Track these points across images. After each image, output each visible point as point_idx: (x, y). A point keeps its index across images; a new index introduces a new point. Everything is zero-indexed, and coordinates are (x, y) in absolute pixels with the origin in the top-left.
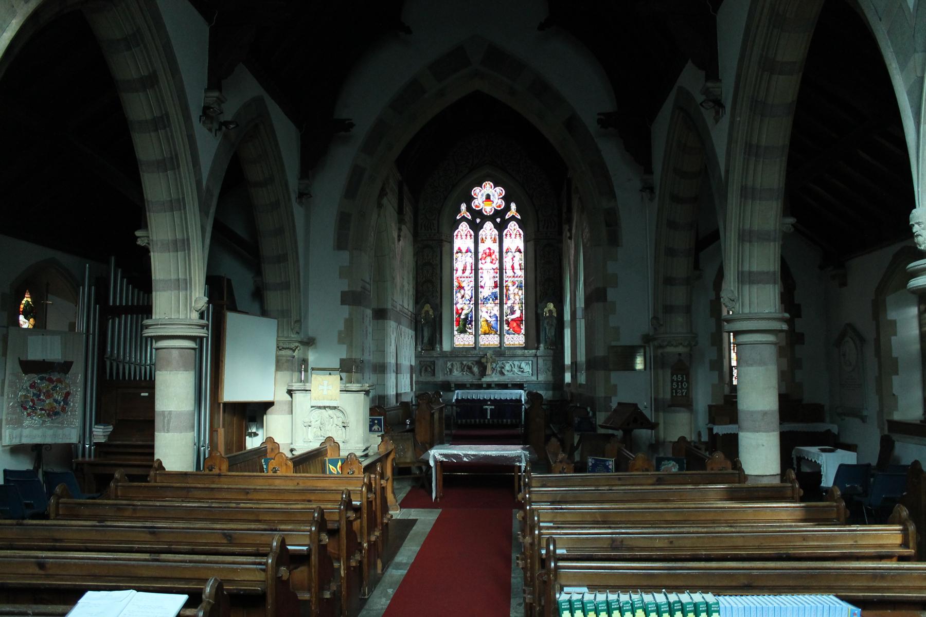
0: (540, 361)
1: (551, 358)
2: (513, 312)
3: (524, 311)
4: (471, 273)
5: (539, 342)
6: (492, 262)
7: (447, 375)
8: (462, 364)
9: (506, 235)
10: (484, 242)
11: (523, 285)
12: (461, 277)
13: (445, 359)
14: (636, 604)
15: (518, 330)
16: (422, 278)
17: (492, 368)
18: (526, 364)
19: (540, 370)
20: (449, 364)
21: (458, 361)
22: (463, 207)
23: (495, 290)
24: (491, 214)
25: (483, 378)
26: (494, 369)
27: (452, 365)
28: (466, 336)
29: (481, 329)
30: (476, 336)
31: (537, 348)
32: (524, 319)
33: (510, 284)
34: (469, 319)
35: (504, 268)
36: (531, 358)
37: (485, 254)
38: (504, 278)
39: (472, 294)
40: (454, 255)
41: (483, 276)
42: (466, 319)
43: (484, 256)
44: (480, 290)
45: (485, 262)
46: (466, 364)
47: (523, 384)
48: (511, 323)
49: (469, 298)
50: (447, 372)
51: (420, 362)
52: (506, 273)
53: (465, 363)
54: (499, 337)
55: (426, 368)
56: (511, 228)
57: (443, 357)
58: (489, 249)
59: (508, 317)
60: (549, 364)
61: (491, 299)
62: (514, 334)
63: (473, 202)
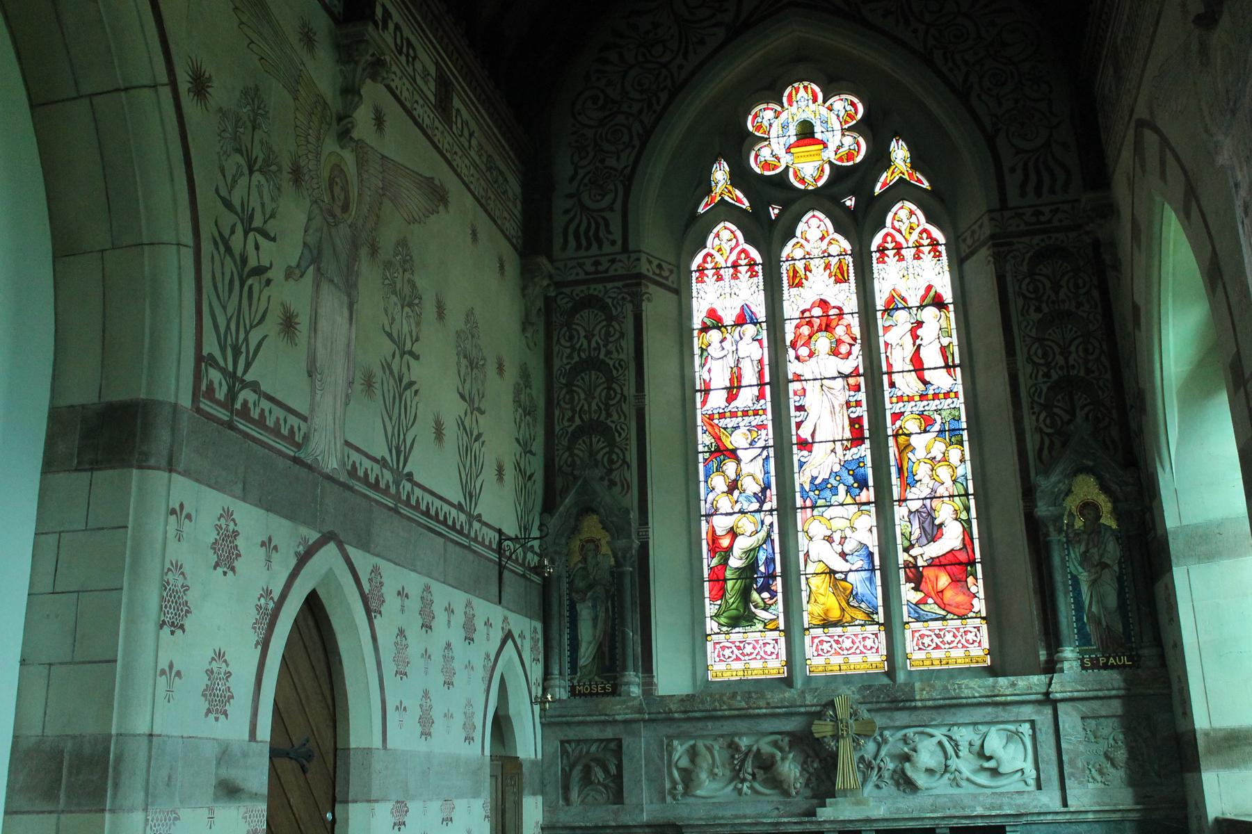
0: (1070, 719)
1: (1116, 706)
2: (933, 532)
3: (974, 523)
4: (761, 396)
5: (1053, 640)
6: (835, 352)
7: (674, 798)
8: (733, 747)
9: (882, 250)
10: (800, 285)
11: (964, 426)
12: (722, 416)
13: (664, 730)
14: (603, 320)
15: (961, 598)
16: (571, 419)
17: (862, 759)
18: (1009, 739)
19: (1072, 761)
20: (680, 749)
21: (716, 738)
22: (720, 174)
23: (855, 453)
24: (820, 184)
25: (823, 805)
26: (869, 766)
27: (693, 754)
28: (753, 634)
30: (792, 631)
31: (1051, 667)
32: (978, 555)
33: (912, 425)
34: (762, 569)
35: (885, 369)
36: (1028, 712)
37: (810, 324)
38: (888, 405)
39: (767, 472)
40: (696, 340)
41: (806, 402)
42: (752, 567)
43: (805, 330)
44: (798, 455)
45: (811, 355)
49: (757, 489)
50: (674, 783)
51: (562, 742)
52: (892, 385)
53: (744, 742)
54: (882, 635)
55: (587, 770)
56: (897, 224)
57: (651, 721)
58: (823, 304)
59: (913, 552)
60: (1110, 730)
61: (842, 489)
62: (943, 619)
63: (753, 154)
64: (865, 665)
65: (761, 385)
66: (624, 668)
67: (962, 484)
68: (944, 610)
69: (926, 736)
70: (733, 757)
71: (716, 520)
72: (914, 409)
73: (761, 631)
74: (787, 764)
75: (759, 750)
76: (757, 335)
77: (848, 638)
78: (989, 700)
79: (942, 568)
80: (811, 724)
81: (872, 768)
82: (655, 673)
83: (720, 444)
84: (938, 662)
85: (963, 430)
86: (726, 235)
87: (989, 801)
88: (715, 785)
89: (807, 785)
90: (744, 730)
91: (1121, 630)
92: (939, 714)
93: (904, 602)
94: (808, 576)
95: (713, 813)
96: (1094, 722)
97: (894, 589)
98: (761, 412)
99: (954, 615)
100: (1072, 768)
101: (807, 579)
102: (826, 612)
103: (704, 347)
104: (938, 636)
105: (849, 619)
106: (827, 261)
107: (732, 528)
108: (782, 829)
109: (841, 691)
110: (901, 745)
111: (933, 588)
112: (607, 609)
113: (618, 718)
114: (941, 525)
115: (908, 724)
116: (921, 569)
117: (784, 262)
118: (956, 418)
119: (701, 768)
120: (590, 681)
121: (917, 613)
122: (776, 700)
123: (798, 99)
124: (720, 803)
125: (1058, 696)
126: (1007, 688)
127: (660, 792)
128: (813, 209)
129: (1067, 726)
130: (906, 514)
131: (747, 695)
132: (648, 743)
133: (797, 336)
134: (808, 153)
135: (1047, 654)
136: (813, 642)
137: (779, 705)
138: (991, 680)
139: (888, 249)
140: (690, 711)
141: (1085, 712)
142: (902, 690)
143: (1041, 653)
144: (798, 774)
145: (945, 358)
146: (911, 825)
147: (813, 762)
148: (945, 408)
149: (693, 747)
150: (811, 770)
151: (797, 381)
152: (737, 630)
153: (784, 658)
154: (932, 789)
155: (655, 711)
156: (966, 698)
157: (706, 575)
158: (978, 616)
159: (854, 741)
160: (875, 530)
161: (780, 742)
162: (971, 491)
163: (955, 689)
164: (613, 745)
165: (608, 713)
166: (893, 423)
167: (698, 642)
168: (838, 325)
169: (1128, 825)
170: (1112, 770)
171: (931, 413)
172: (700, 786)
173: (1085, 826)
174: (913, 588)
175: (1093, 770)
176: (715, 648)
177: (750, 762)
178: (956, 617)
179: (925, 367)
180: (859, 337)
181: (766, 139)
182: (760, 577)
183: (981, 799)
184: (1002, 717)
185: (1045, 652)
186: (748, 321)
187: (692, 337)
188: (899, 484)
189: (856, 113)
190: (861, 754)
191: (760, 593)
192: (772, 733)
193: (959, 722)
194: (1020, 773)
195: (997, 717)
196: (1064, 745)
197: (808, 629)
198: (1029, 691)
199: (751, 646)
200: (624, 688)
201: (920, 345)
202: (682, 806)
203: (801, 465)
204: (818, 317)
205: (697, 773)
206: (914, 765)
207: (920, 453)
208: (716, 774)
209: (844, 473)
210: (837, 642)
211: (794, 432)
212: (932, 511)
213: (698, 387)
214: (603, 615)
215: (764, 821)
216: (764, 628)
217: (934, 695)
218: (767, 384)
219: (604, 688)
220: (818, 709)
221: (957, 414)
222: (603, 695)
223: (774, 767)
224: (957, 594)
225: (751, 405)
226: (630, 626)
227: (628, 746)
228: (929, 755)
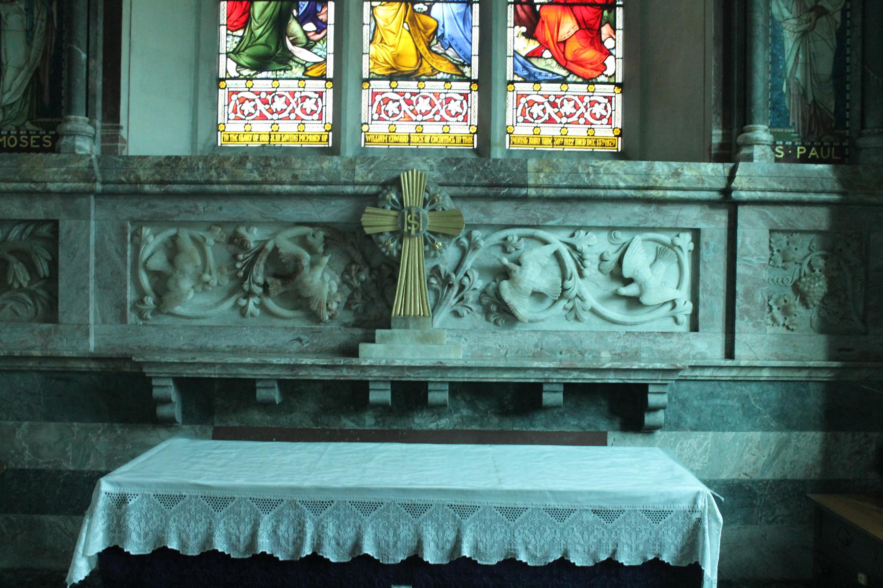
1: (820, 218)
7: (141, 315)
8: (236, 242)
13: (128, 210)
15: (589, 54)
17: (436, 270)
19: (748, 294)
21: (211, 226)
26: (447, 283)
27: (173, 249)
29: (374, 50)
36: (692, 216)
46: (263, 244)
47: (643, 389)
50: (141, 294)
53: (254, 236)
54: (474, 97)
62: (563, 81)
64: (445, 137)
66: (70, 110)
68: (565, 68)
69: (535, 242)
70: (235, 257)
73: (300, 79)
74: (319, 272)
75: (276, 249)
77: (425, 97)
78: (639, 194)
79: (568, 9)
80: (359, 213)
81: (451, 286)
82: (123, 122)
84: (550, 141)
87: (621, 344)
88: (204, 300)
89: (347, 306)
90: (256, 217)
91: (832, 109)
92: (560, 210)
93: (510, 52)
95: (198, 343)
96: (784, 238)
97: (499, 29)
99: (579, 77)
100: (748, 303)
102: (396, 57)
104: (553, 105)
105: (429, 70)
108: (303, 374)
109: (408, 165)
110: (497, 252)
111: (552, 37)
112: (50, 16)
113: (52, 187)
115: (510, 223)
116: (538, 7)
119: (183, 272)
120: (18, 129)
121: (527, 69)
122: (308, 172)
124: (211, 328)
125: (744, 195)
126: (667, 178)
127: (117, 307)
129: (748, 240)
131: (262, 162)
132: (101, 231)
135: (723, 135)
136: (373, 101)
137: (313, 180)
140: (170, 183)
141: (777, 224)
142: (509, 170)
143: (714, 132)
144: (335, 289)
146: (506, 377)
147: (359, 271)
149: (174, 239)
150: (356, 284)
152: (264, 74)
153: (330, 119)
154: (537, 321)
155: (113, 179)
156: (604, 188)
158: (612, 80)
159: (426, 243)
161: (310, 239)
163: (588, 174)
164: (44, 230)
165: (34, 178)
167: (203, 89)
169: (812, 387)
170: (800, 309)
172: (178, 300)
173: (754, 387)
174: (523, 34)
175: (775, 308)
176: (230, 100)
177: (262, 267)
178: (580, 80)
183: (610, 340)
184: (653, 221)
185: (720, 132)
190: (435, 264)
192: (299, 224)
193: (592, 223)
194: (669, 306)
195: (646, 221)
196: (740, 269)
197: (368, 80)
198: (700, 186)
199: (284, 99)
200: (64, 141)
202: (153, 329)
205: (176, 280)
206: (515, 285)
208: (207, 283)
210: (409, 102)
214: (44, 25)
215: (275, 361)
216: (303, 74)
217: (557, 180)
219: (39, 141)
220: (374, 189)
222: (37, 151)
223: (298, 278)
224: (585, 48)
226: (83, 42)
227: (69, 232)
228: (540, 270)
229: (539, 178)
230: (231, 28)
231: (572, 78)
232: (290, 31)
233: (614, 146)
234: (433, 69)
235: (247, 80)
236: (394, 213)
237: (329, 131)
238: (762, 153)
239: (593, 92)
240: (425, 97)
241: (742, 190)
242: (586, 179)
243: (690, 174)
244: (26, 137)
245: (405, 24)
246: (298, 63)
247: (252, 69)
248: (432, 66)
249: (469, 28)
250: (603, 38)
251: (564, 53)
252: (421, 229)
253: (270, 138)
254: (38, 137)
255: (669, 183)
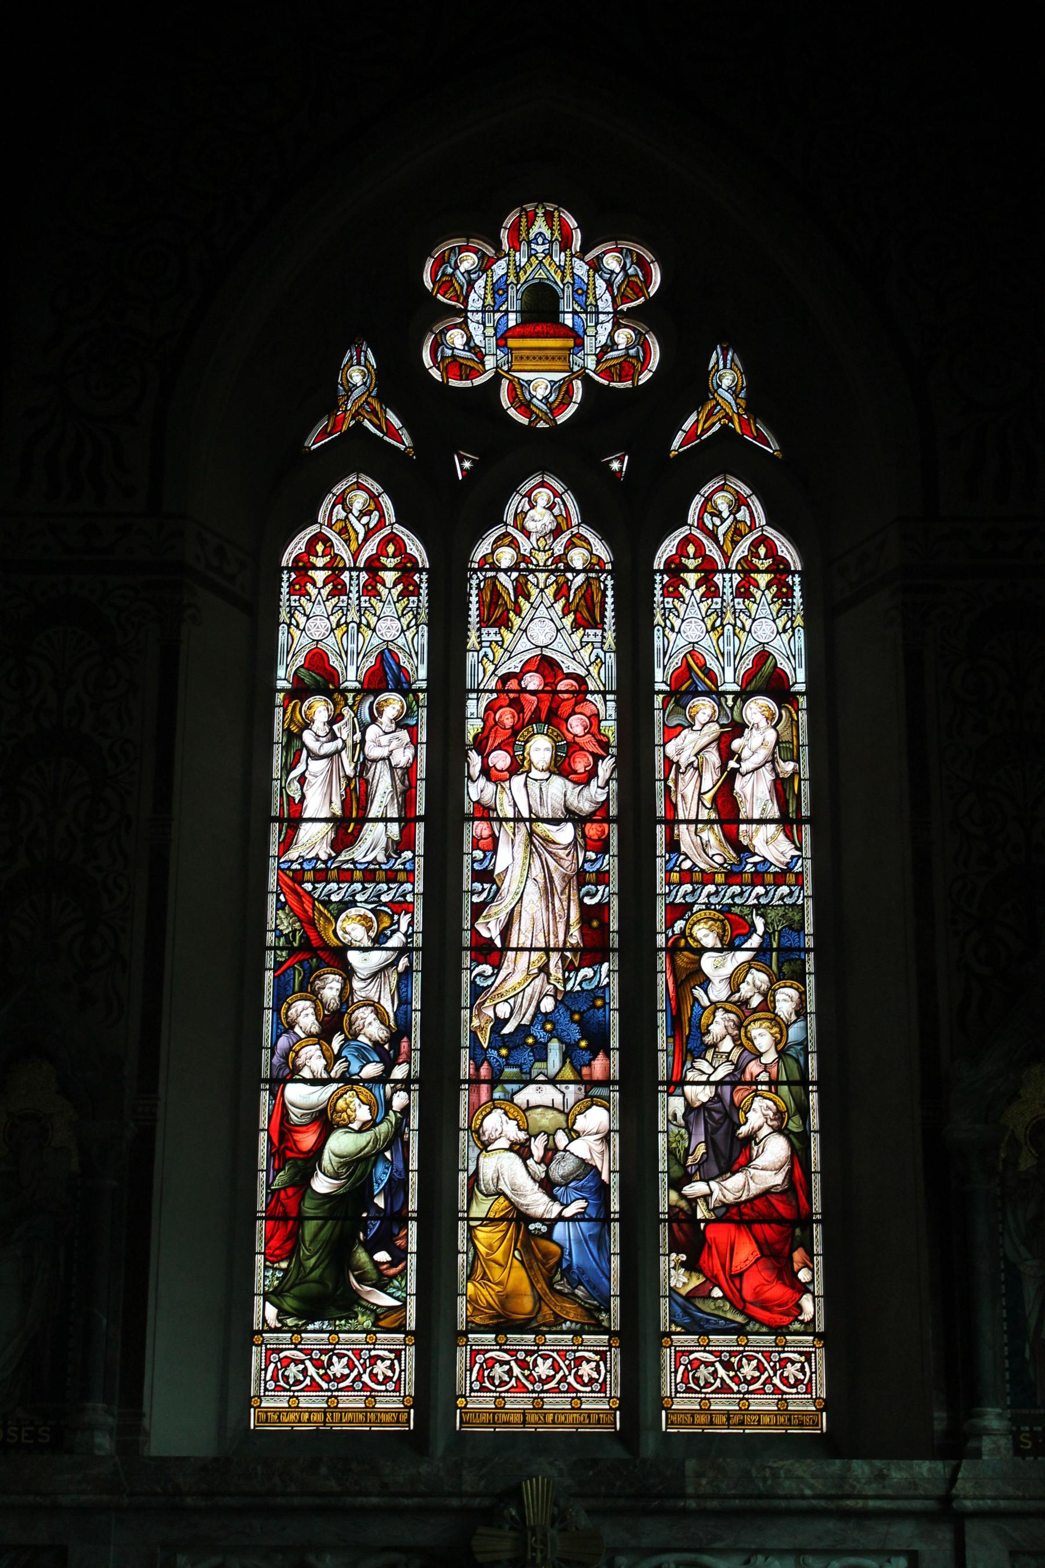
4: (406, 842)
6: (560, 767)
9: (675, 569)
10: (504, 622)
11: (810, 942)
12: (321, 876)
15: (776, 1291)
32: (817, 1206)
33: (705, 935)
35: (661, 811)
36: (905, 1533)
37: (516, 704)
38: (661, 888)
40: (279, 712)
43: (507, 717)
48: (720, 1235)
52: (673, 846)
54: (615, 1355)
58: (546, 666)
61: (555, 1050)
62: (740, 1330)
65: (406, 820)
67: (797, 1061)
68: (742, 1312)
71: (295, 1093)
72: (713, 900)
76: (407, 716)
78: (831, 1505)
82: (146, 1409)
83: (312, 934)
85: (808, 951)
86: (359, 501)
93: (664, 1291)
94: (473, 1223)
98: (402, 876)
99: (762, 1324)
101: (471, 1229)
102: (505, 1299)
103: (294, 729)
106: (561, 580)
107: (324, 1111)
111: (723, 1267)
114: (752, 1137)
116: (702, 1225)
117: (475, 571)
118: (795, 926)
123: (532, 236)
126: (869, 1482)
128: (359, 471)
130: (680, 1111)
133: (490, 726)
134: (536, 353)
138: (838, 1463)
139: (314, 568)
143: (936, 1415)
145: (783, 806)
148: (775, 902)
151: (481, 819)
153: (411, 1390)
157: (261, 1205)
160: (615, 1139)
162: (813, 1074)
163: (765, 1479)
166: (670, 925)
168: (574, 713)
171: (746, 911)
174: (683, 1264)
176: (268, 1362)
179: (742, 816)
180: (613, 740)
181: (458, 312)
182: (375, 1219)
186: (391, 686)
187: (270, 707)
188: (671, 1048)
189: (648, 280)
191: (371, 1253)
198: (911, 1492)
201: (735, 772)
203: (477, 991)
204: (533, 693)
207: (719, 991)
209: (563, 1018)
211: (467, 925)
212: (734, 1111)
213: (275, 812)
216: (374, 1325)
218: (420, 819)
220: (487, 1502)
221: (797, 918)
225: (381, 858)
229: (700, 1485)
230: (271, 1259)
231: (753, 1326)
232: (355, 1262)
233: (817, 1425)
234: (557, 1316)
235: (294, 1333)
236: (513, 1534)
237: (410, 1408)
238: (994, 1446)
239: (784, 1347)
240: (545, 1357)
241: (965, 1498)
242: (761, 1485)
243: (899, 1477)
244: (16, 1429)
245: (516, 1253)
246: (367, 1308)
247: (300, 1318)
248: (554, 1313)
249: (606, 1257)
250: (796, 1267)
251: (740, 1291)
252: (549, 1556)
253: (325, 1417)
254: (32, 1428)
255: (871, 1489)
